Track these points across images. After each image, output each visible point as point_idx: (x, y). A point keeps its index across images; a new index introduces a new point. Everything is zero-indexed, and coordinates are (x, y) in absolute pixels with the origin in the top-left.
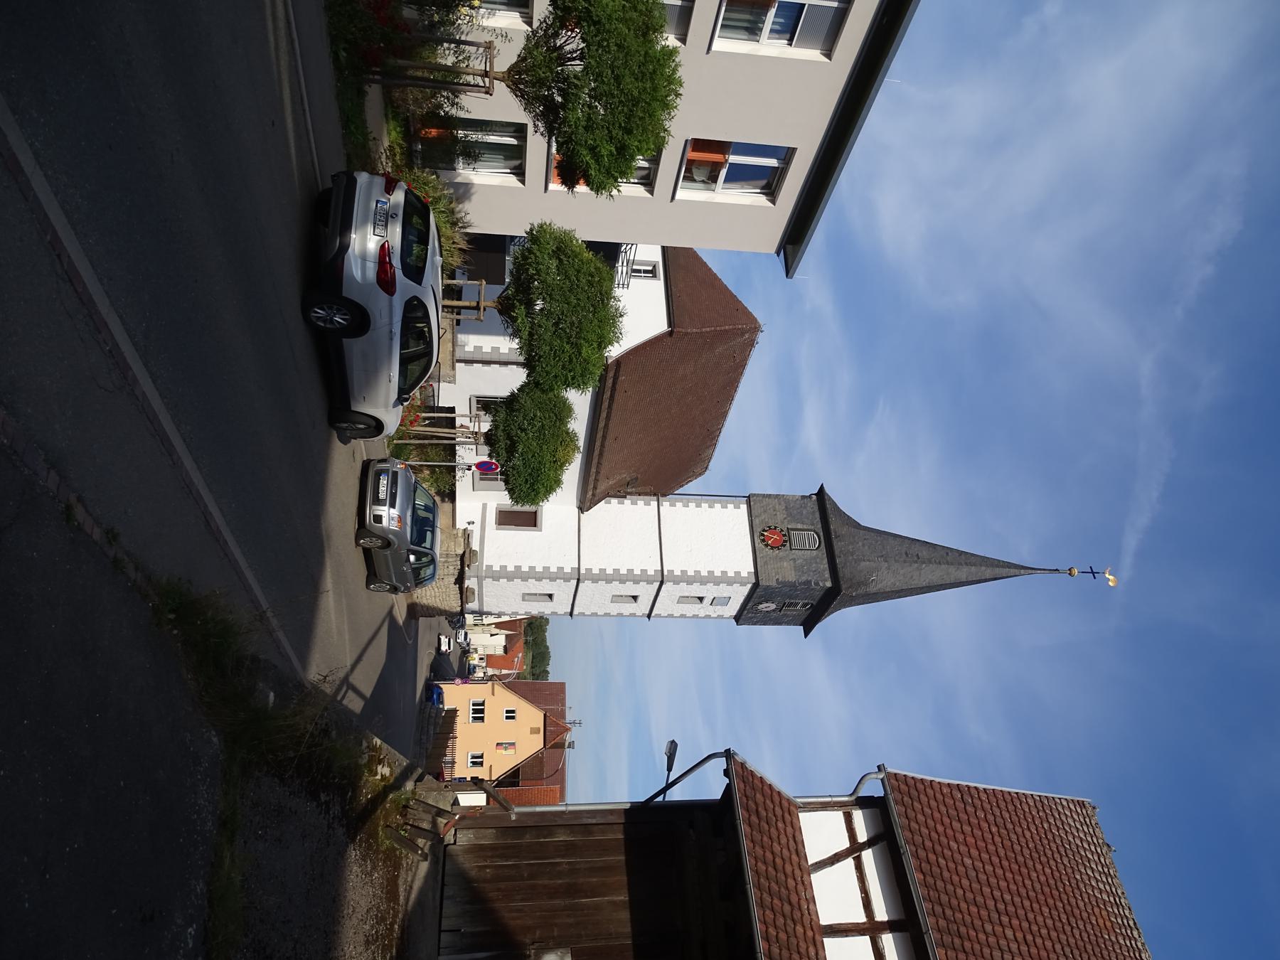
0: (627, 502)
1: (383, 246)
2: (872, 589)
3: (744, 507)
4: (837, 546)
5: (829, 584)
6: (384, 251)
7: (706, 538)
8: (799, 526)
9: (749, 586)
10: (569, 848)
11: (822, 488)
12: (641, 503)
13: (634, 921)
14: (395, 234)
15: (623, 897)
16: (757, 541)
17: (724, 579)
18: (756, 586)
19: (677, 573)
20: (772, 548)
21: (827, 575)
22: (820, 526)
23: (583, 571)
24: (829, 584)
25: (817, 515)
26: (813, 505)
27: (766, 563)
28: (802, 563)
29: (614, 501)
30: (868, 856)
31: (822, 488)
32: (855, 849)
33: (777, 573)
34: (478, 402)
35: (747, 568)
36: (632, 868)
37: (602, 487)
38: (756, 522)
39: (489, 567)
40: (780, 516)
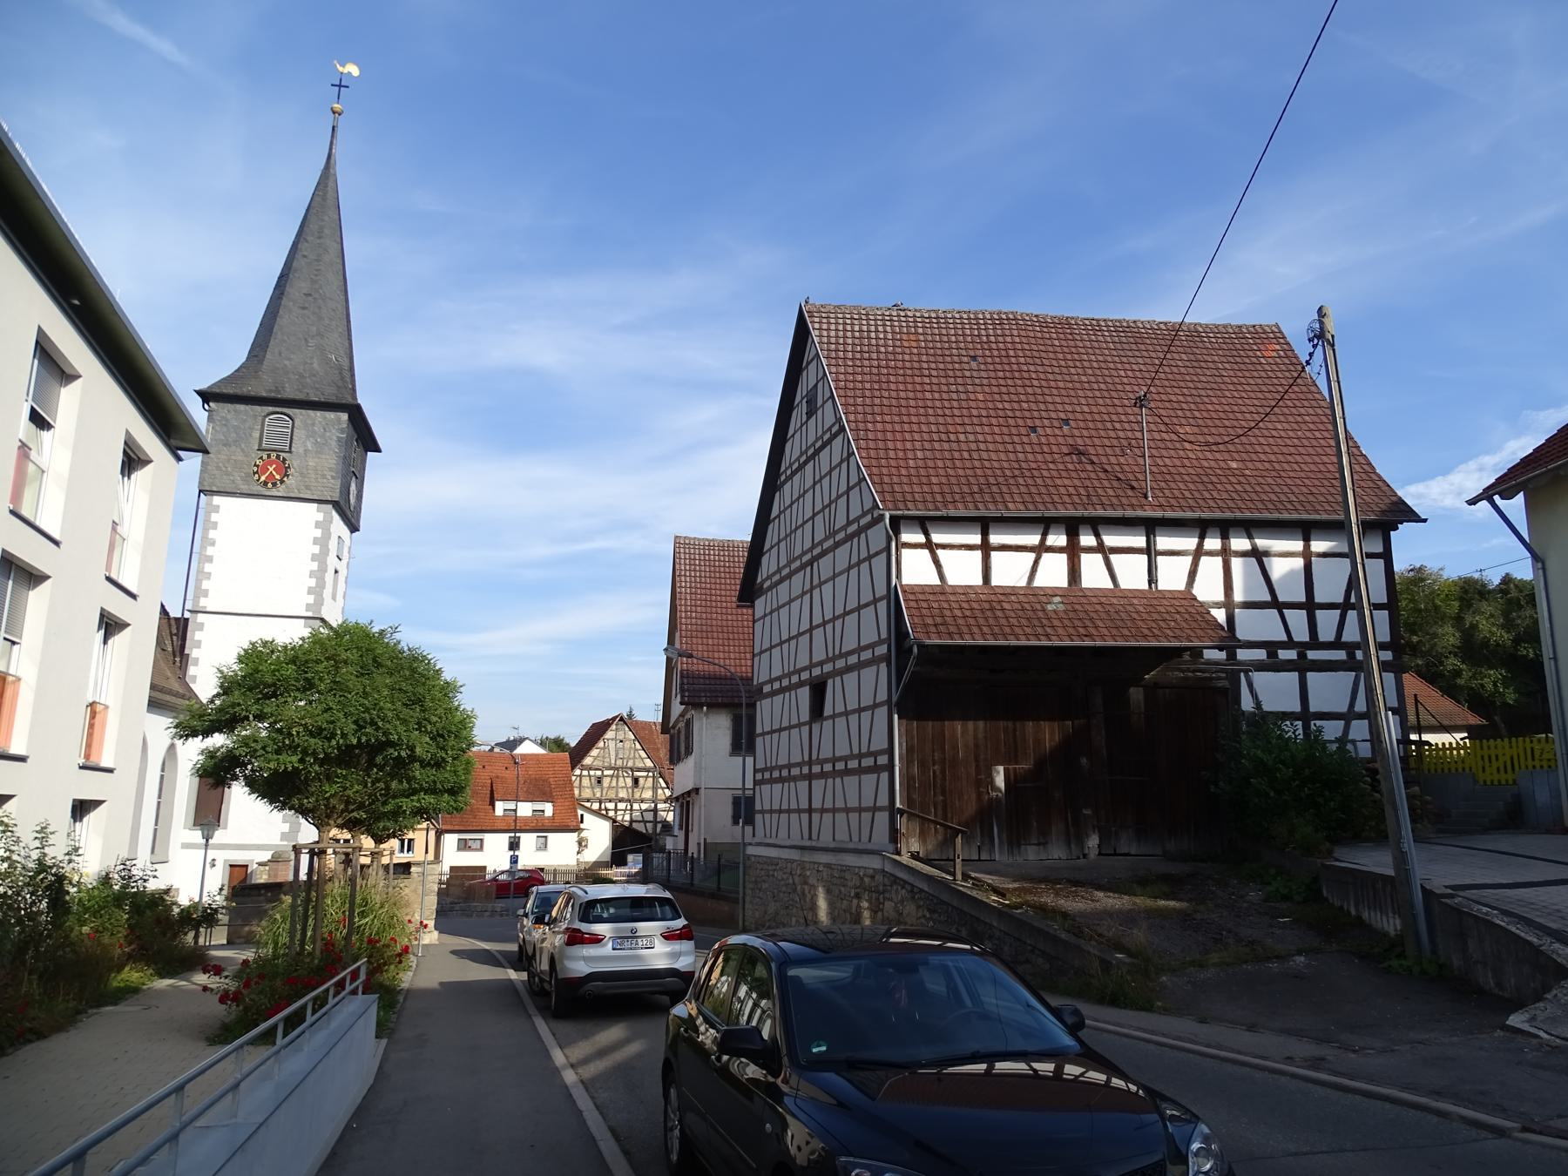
1: (666, 938)
2: (346, 364)
3: (217, 500)
4: (290, 392)
6: (669, 936)
8: (257, 435)
9: (334, 513)
10: (922, 764)
11: (199, 393)
12: (198, 636)
13: (976, 719)
14: (644, 927)
15: (959, 726)
16: (274, 492)
17: (322, 542)
18: (336, 505)
19: (311, 599)
21: (331, 415)
22: (258, 408)
25: (242, 407)
27: (307, 488)
30: (937, 538)
31: (199, 393)
32: (929, 546)
33: (324, 476)
34: (1386, 837)
35: (310, 513)
36: (942, 719)
37: (176, 686)
38: (245, 488)
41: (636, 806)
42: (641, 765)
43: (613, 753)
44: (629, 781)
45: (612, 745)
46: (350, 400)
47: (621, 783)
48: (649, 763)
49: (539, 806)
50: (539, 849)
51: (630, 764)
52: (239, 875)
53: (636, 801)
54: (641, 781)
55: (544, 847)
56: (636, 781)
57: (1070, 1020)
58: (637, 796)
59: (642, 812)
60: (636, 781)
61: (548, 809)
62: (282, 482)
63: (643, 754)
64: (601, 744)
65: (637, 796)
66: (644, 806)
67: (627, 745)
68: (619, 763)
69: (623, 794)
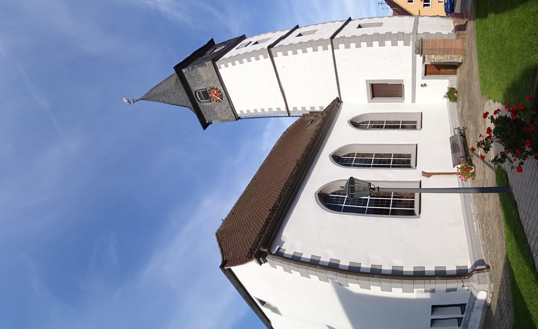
0: (308, 109)
3: (238, 112)
5: (184, 70)
7: (250, 84)
16: (223, 91)
20: (213, 88)
23: (330, 46)
24: (184, 70)
26: (415, 146)
28: (200, 76)
29: (317, 109)
39: (406, 44)
40: (217, 109)
62: (216, 89)
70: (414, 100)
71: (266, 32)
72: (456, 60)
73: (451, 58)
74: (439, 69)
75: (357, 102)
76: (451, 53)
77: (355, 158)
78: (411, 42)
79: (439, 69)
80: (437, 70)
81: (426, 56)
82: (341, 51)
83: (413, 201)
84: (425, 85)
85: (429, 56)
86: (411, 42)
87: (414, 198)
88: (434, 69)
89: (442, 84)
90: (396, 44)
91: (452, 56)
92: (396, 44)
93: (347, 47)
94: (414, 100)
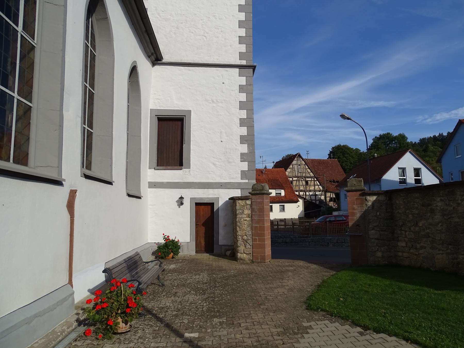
23: (244, 63)
41: (307, 193)
42: (308, 175)
43: (296, 170)
44: (304, 182)
45: (296, 167)
46: (161, 122)
47: (301, 183)
48: (312, 174)
49: (278, 191)
50: (281, 211)
51: (304, 175)
52: (206, 212)
53: (307, 191)
54: (309, 182)
55: (283, 209)
56: (307, 182)
57: (228, 253)
58: (308, 189)
59: (310, 196)
60: (307, 182)
61: (283, 193)
63: (309, 171)
64: (291, 166)
65: (308, 189)
66: (311, 193)
67: (302, 167)
68: (299, 175)
69: (302, 188)
70: (153, 185)
71: (5, 120)
72: (241, 248)
73: (246, 241)
74: (205, 224)
75: (162, 91)
76: (254, 240)
77: (15, 95)
78: (247, 181)
79: (205, 224)
80: (203, 220)
81: (249, 202)
82: (235, 78)
83: (8, 160)
84: (182, 204)
85: (248, 207)
86: (247, 181)
87: (14, 162)
88: (206, 217)
89: (181, 229)
90: (243, 160)
91: (250, 242)
92: (243, 160)
93: (242, 89)
94: (153, 185)
